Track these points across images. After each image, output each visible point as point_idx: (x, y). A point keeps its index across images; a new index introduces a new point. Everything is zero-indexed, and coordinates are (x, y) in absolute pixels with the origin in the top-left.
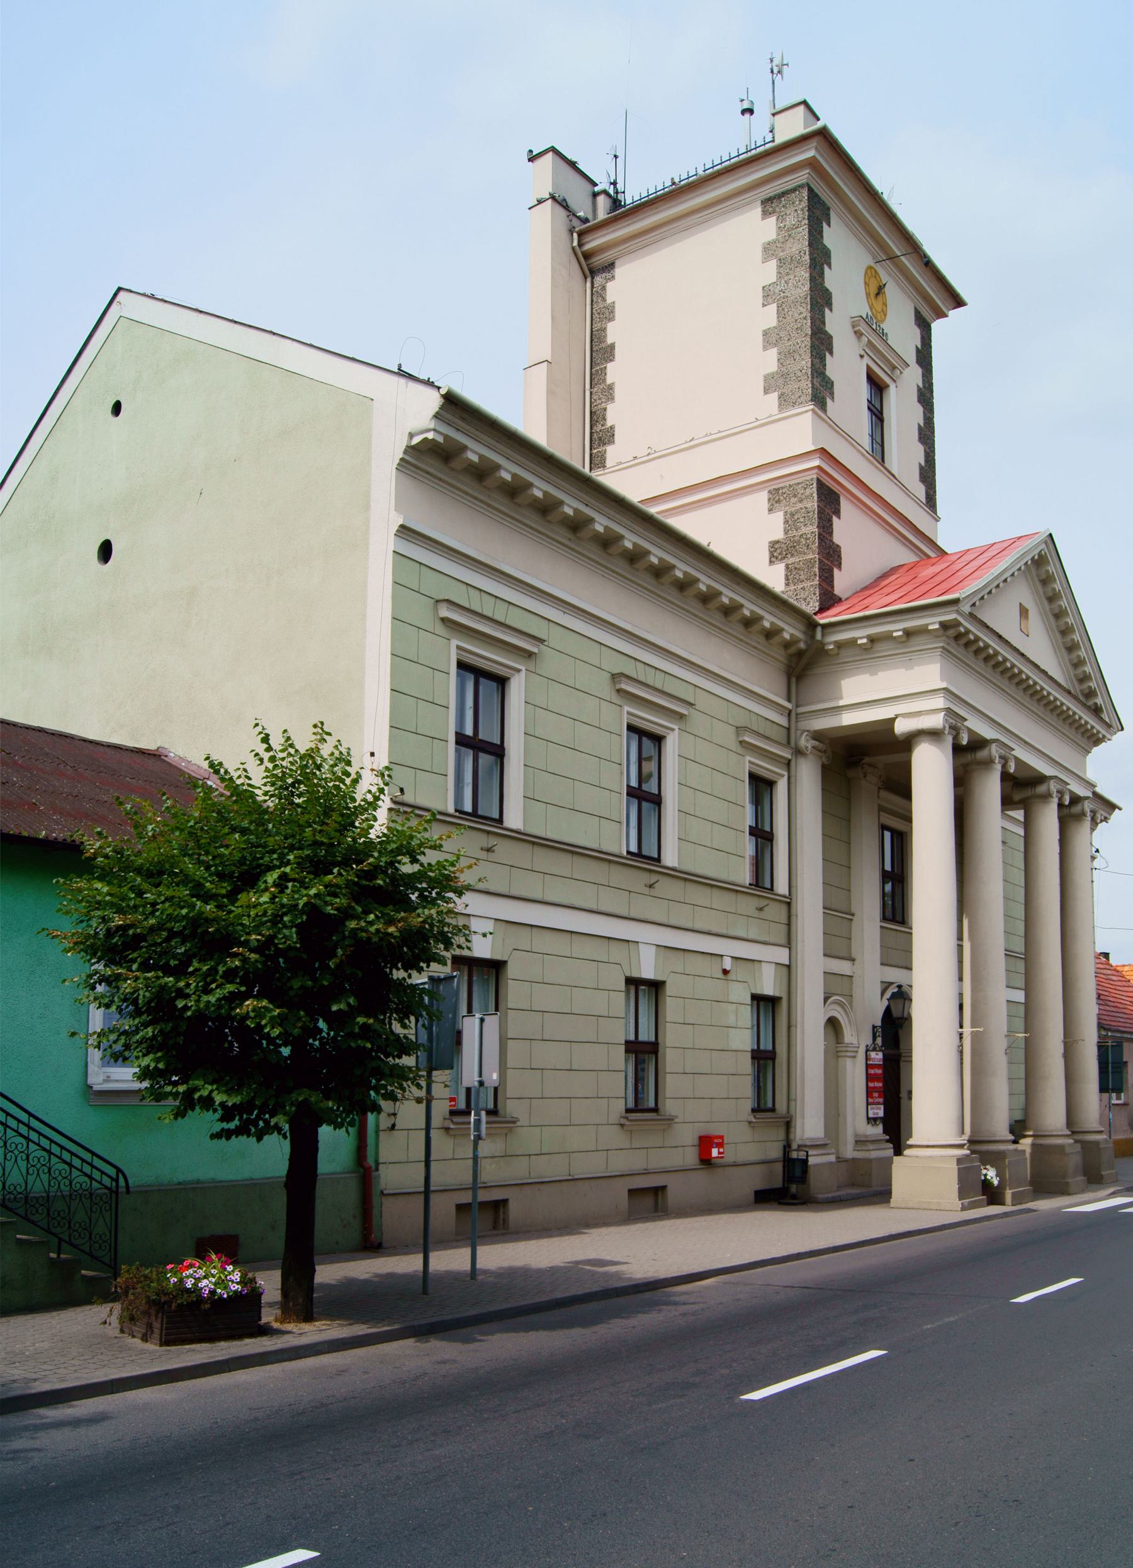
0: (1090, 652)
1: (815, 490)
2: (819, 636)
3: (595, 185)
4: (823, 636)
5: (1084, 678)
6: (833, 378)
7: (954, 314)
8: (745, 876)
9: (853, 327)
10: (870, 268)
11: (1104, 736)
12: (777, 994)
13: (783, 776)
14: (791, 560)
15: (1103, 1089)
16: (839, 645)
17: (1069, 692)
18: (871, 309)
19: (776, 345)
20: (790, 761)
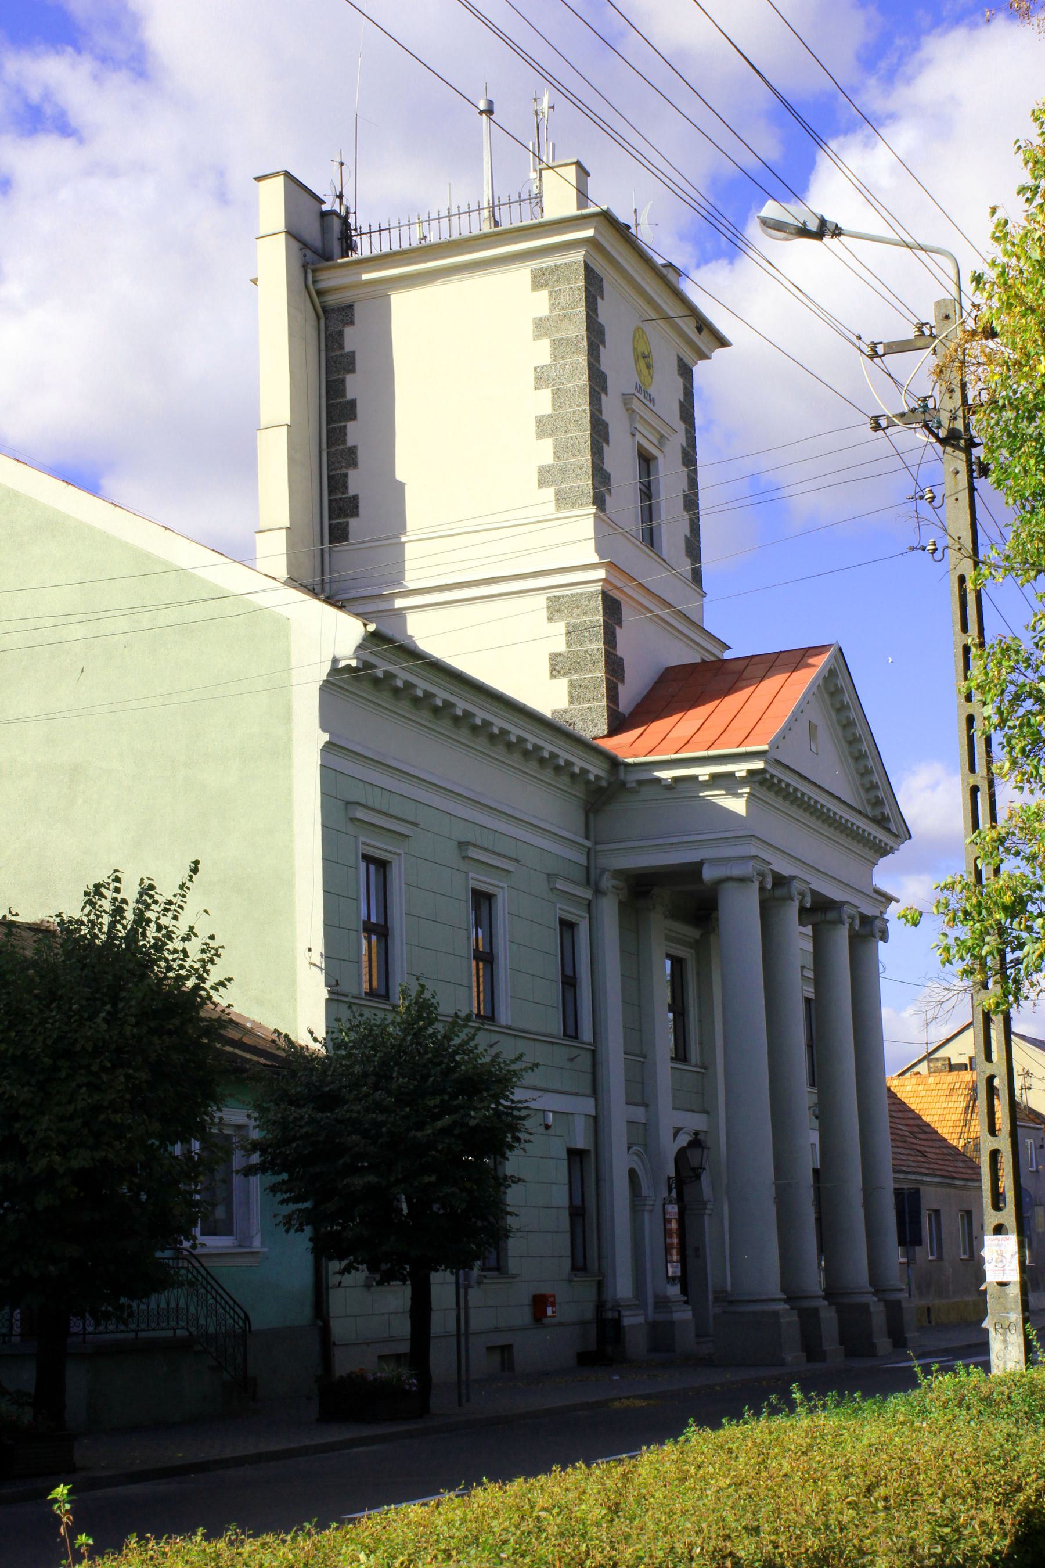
0: (854, 696)
1: (600, 603)
2: (622, 776)
3: (323, 202)
4: (625, 774)
5: (878, 803)
6: (609, 470)
7: (719, 353)
8: (555, 1026)
9: (625, 405)
10: (638, 329)
11: (892, 848)
12: (587, 1148)
13: (584, 918)
14: (576, 677)
15: (902, 1242)
16: (641, 783)
17: (859, 812)
18: (639, 376)
19: (551, 435)
20: (590, 901)
